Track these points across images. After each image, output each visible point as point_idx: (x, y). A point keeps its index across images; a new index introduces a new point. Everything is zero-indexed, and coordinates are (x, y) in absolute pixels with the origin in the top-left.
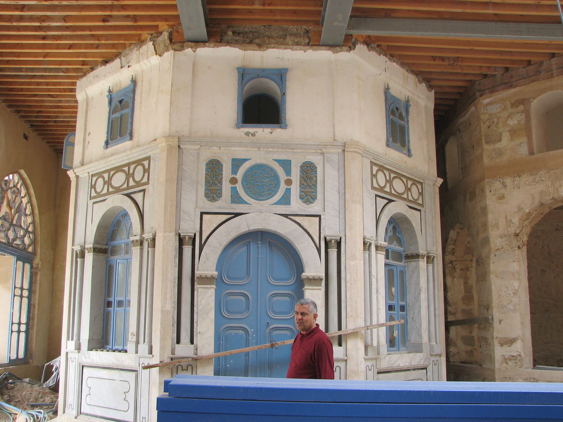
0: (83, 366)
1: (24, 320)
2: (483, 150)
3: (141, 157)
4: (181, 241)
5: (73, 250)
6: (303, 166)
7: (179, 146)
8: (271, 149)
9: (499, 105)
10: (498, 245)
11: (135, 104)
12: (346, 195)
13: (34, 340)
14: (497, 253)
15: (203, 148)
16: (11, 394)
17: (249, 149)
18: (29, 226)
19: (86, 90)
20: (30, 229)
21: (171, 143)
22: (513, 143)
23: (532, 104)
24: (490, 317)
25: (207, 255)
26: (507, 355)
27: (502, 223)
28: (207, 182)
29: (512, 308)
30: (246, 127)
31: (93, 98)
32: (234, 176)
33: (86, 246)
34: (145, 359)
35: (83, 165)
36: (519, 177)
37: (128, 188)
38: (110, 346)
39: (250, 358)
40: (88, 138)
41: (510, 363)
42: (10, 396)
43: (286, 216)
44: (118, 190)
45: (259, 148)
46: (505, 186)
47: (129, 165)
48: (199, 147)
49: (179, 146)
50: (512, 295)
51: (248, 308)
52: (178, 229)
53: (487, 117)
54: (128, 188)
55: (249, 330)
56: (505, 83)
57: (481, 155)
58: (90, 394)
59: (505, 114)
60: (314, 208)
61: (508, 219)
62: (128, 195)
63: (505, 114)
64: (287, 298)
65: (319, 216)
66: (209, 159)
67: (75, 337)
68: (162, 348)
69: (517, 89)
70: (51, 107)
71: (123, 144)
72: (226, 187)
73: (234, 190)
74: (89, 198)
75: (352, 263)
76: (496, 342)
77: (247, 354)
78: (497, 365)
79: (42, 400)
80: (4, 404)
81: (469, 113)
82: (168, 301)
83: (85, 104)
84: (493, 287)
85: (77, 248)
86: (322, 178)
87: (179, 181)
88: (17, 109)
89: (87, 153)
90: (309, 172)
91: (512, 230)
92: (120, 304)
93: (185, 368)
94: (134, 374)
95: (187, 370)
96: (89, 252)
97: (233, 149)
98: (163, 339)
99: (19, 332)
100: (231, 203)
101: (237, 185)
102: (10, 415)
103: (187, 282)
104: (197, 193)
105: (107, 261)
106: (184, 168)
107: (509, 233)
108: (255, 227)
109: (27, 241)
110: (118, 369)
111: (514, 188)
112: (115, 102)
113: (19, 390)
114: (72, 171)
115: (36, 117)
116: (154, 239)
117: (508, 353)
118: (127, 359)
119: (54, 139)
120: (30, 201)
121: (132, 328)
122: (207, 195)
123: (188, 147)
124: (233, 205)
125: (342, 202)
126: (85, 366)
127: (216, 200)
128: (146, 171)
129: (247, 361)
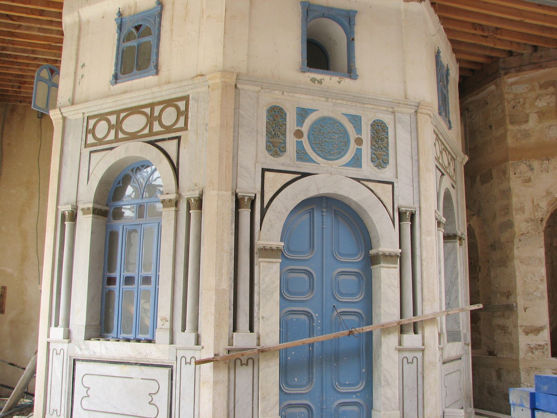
0: (74, 360)
2: (506, 131)
4: (238, 203)
5: (57, 209)
6: (374, 125)
7: (236, 85)
8: (339, 101)
10: (523, 229)
11: (162, 33)
12: (421, 161)
15: (263, 91)
17: (316, 98)
19: (80, 10)
22: (541, 125)
24: (514, 304)
25: (270, 221)
27: (528, 206)
28: (268, 132)
29: (539, 295)
30: (311, 72)
31: (88, 21)
33: (81, 206)
34: (188, 352)
35: (73, 103)
37: (151, 133)
38: (114, 334)
40: (80, 72)
41: (537, 353)
43: (358, 180)
44: (133, 136)
45: (327, 98)
46: (532, 170)
47: (152, 106)
48: (258, 89)
49: (236, 85)
50: (539, 282)
51: (311, 287)
52: (234, 187)
53: (510, 97)
54: (151, 133)
55: (313, 314)
56: (534, 63)
57: (504, 137)
58: (88, 396)
59: (533, 95)
60: (387, 174)
61: (535, 203)
62: (152, 143)
63: (533, 95)
64: (353, 278)
65: (392, 183)
67: (61, 322)
68: (217, 337)
69: (546, 70)
71: (143, 80)
72: (291, 141)
73: (300, 145)
74: (83, 146)
75: (428, 239)
76: (520, 331)
77: (311, 345)
78: (521, 355)
81: (486, 91)
82: (224, 278)
84: (517, 273)
85: (66, 208)
86: (393, 140)
87: (237, 126)
89: (78, 89)
90: (379, 131)
91: (539, 215)
92: (146, 280)
93: (244, 361)
94: (167, 371)
95: (247, 364)
96: (84, 214)
97: (297, 95)
98: (218, 326)
100: (297, 160)
101: (302, 139)
103: (245, 254)
105: (107, 227)
107: (536, 218)
108: (324, 191)
110: (136, 364)
111: (542, 171)
112: (129, 27)
114: (57, 111)
117: (534, 342)
121: (164, 311)
122: (268, 149)
123: (246, 87)
124: (298, 162)
125: (415, 169)
126: (78, 360)
127: (279, 156)
128: (183, 114)
129: (311, 353)
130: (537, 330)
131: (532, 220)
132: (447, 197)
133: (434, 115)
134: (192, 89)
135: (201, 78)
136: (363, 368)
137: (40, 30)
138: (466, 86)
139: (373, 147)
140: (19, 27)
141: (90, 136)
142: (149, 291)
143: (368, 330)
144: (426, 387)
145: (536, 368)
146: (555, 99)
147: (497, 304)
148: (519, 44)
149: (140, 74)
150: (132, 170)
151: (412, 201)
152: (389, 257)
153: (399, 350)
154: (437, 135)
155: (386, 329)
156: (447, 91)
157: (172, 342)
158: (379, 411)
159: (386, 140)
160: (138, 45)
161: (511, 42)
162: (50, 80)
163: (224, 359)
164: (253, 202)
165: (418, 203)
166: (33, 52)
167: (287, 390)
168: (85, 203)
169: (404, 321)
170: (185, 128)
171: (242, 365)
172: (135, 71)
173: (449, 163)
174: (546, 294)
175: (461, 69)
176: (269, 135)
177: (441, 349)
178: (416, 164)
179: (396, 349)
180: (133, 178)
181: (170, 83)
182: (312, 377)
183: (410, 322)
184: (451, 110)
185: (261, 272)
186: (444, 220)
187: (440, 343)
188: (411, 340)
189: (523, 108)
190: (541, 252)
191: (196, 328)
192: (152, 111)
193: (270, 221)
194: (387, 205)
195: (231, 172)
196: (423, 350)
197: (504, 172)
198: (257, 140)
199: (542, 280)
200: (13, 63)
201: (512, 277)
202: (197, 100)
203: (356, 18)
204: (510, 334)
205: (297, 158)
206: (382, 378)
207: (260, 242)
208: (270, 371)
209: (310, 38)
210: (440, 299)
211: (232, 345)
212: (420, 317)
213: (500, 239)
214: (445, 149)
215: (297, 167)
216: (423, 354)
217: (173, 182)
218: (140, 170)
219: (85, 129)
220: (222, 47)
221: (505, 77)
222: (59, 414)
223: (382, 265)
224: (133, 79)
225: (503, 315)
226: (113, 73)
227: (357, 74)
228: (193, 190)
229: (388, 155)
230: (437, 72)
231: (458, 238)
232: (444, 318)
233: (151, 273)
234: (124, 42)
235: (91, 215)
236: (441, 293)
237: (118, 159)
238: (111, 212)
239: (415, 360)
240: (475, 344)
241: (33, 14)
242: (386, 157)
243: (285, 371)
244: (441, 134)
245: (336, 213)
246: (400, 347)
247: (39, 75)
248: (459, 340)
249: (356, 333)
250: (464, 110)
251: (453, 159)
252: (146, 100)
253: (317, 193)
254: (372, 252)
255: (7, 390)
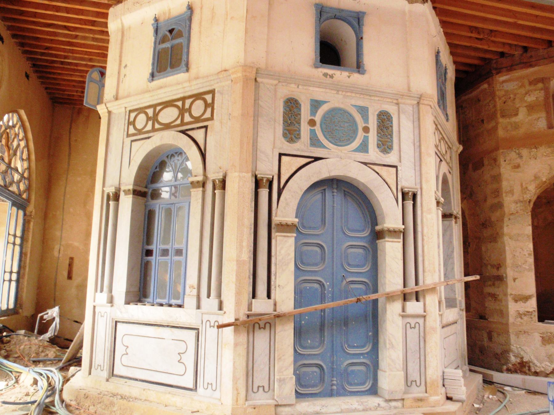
0: (116, 322)
1: (15, 269)
2: (497, 123)
3: (202, 90)
4: (258, 183)
5: (103, 191)
7: (256, 79)
8: (349, 94)
9: (515, 83)
13: (25, 289)
14: (512, 217)
15: (280, 84)
16: (7, 349)
17: (328, 90)
18: (25, 172)
19: (123, 18)
20: (26, 175)
21: (248, 74)
22: (530, 118)
23: (551, 82)
24: (504, 275)
25: (286, 199)
26: (522, 310)
27: (517, 189)
28: (285, 121)
29: (527, 267)
30: (324, 68)
31: (130, 28)
32: (313, 118)
33: (123, 188)
34: (212, 316)
35: (116, 98)
36: (536, 148)
37: (183, 124)
38: (150, 300)
39: (326, 314)
40: (123, 71)
41: (525, 318)
42: (7, 351)
43: (365, 164)
44: (167, 127)
45: (338, 91)
46: (521, 157)
47: (183, 99)
48: (275, 82)
49: (256, 79)
50: (527, 256)
51: (323, 259)
52: (254, 170)
55: (325, 283)
56: (523, 63)
57: (495, 128)
58: (127, 354)
60: (391, 158)
61: (524, 187)
62: (183, 132)
63: (523, 91)
64: (361, 251)
66: (287, 97)
67: (106, 289)
68: (238, 303)
69: (536, 68)
70: (63, 43)
71: (176, 76)
72: (305, 129)
73: (313, 133)
74: (125, 136)
75: (429, 216)
76: (510, 298)
77: (323, 311)
78: (511, 320)
79: (43, 354)
80: (5, 362)
81: (479, 90)
82: (244, 250)
83: (120, 34)
84: (507, 248)
85: (110, 190)
86: (397, 129)
87: (256, 116)
88: (23, 41)
90: (384, 120)
91: (527, 197)
92: (179, 252)
94: (194, 333)
95: (264, 328)
97: (311, 88)
98: (238, 293)
99: (10, 281)
101: (315, 128)
102: (10, 374)
103: (263, 228)
104: (275, 132)
105: (146, 206)
106: (261, 103)
107: (525, 199)
109: (22, 187)
110: (168, 326)
112: (164, 31)
113: (15, 344)
114: (103, 105)
115: (43, 54)
116: (223, 182)
118: (186, 315)
119: (53, 84)
120: (27, 146)
122: (285, 135)
123: (265, 81)
124: (312, 148)
125: (417, 154)
126: (119, 322)
129: (323, 318)
130: (526, 299)
131: (522, 202)
132: (445, 181)
133: (434, 106)
134: (218, 83)
135: (225, 72)
136: (370, 332)
137: (94, 39)
138: (461, 87)
139: (379, 135)
140: (76, 37)
141: (131, 127)
142: (180, 262)
143: (374, 298)
144: (428, 350)
145: (525, 332)
146: (543, 94)
147: (488, 274)
148: (510, 45)
149: (173, 72)
150: (167, 157)
151: (414, 182)
152: (394, 233)
153: (403, 316)
154: (436, 125)
155: (390, 297)
156: (445, 88)
157: (198, 307)
158: (385, 372)
159: (390, 128)
160: (171, 47)
161: (504, 44)
162: (100, 81)
163: (244, 323)
164: (271, 183)
165: (419, 185)
166: (91, 60)
167: (301, 351)
168: (126, 185)
169: (407, 290)
170: (212, 118)
171: (260, 328)
172: (169, 69)
173: (446, 152)
174: (533, 267)
175: (457, 71)
176: (286, 124)
177: (441, 315)
178: (418, 150)
179: (400, 315)
180: (168, 164)
181: (198, 78)
182: (324, 340)
183: (413, 291)
184: (448, 104)
185: (278, 245)
186: (442, 200)
187: (440, 311)
188: (413, 307)
189: (514, 103)
190: (529, 230)
191: (219, 295)
192: (183, 104)
193: (286, 199)
194: (391, 186)
195: (251, 156)
196: (424, 317)
197: (495, 160)
198: (275, 128)
199: (529, 254)
200: (74, 70)
201: (502, 252)
202: (222, 94)
203: (365, 19)
204: (501, 301)
205: (311, 144)
206: (387, 342)
207: (276, 218)
208: (285, 335)
209: (323, 40)
210: (440, 271)
211: (251, 311)
212: (421, 286)
213: (490, 218)
214: (443, 138)
215: (311, 152)
216: (425, 320)
217: (201, 166)
218: (174, 156)
219: (127, 122)
220: (243, 44)
221: (497, 76)
222: (102, 369)
223: (387, 239)
224: (167, 77)
225: (494, 284)
226: (150, 71)
227: (365, 69)
228: (218, 173)
229: (392, 141)
230: (437, 70)
231: (453, 217)
232: (443, 287)
233: (182, 246)
234: (159, 44)
235: (131, 196)
236: (440, 265)
237: (154, 147)
238: (149, 194)
239: (417, 325)
240: (468, 308)
241: (86, 24)
242: (390, 144)
243: (299, 333)
244: (440, 124)
245: (345, 194)
246: (404, 313)
247: (90, 76)
248: (455, 307)
249: (364, 300)
250: (459, 108)
251: (450, 148)
252: (179, 94)
253: (328, 176)
254: (378, 228)
255: (67, 343)
